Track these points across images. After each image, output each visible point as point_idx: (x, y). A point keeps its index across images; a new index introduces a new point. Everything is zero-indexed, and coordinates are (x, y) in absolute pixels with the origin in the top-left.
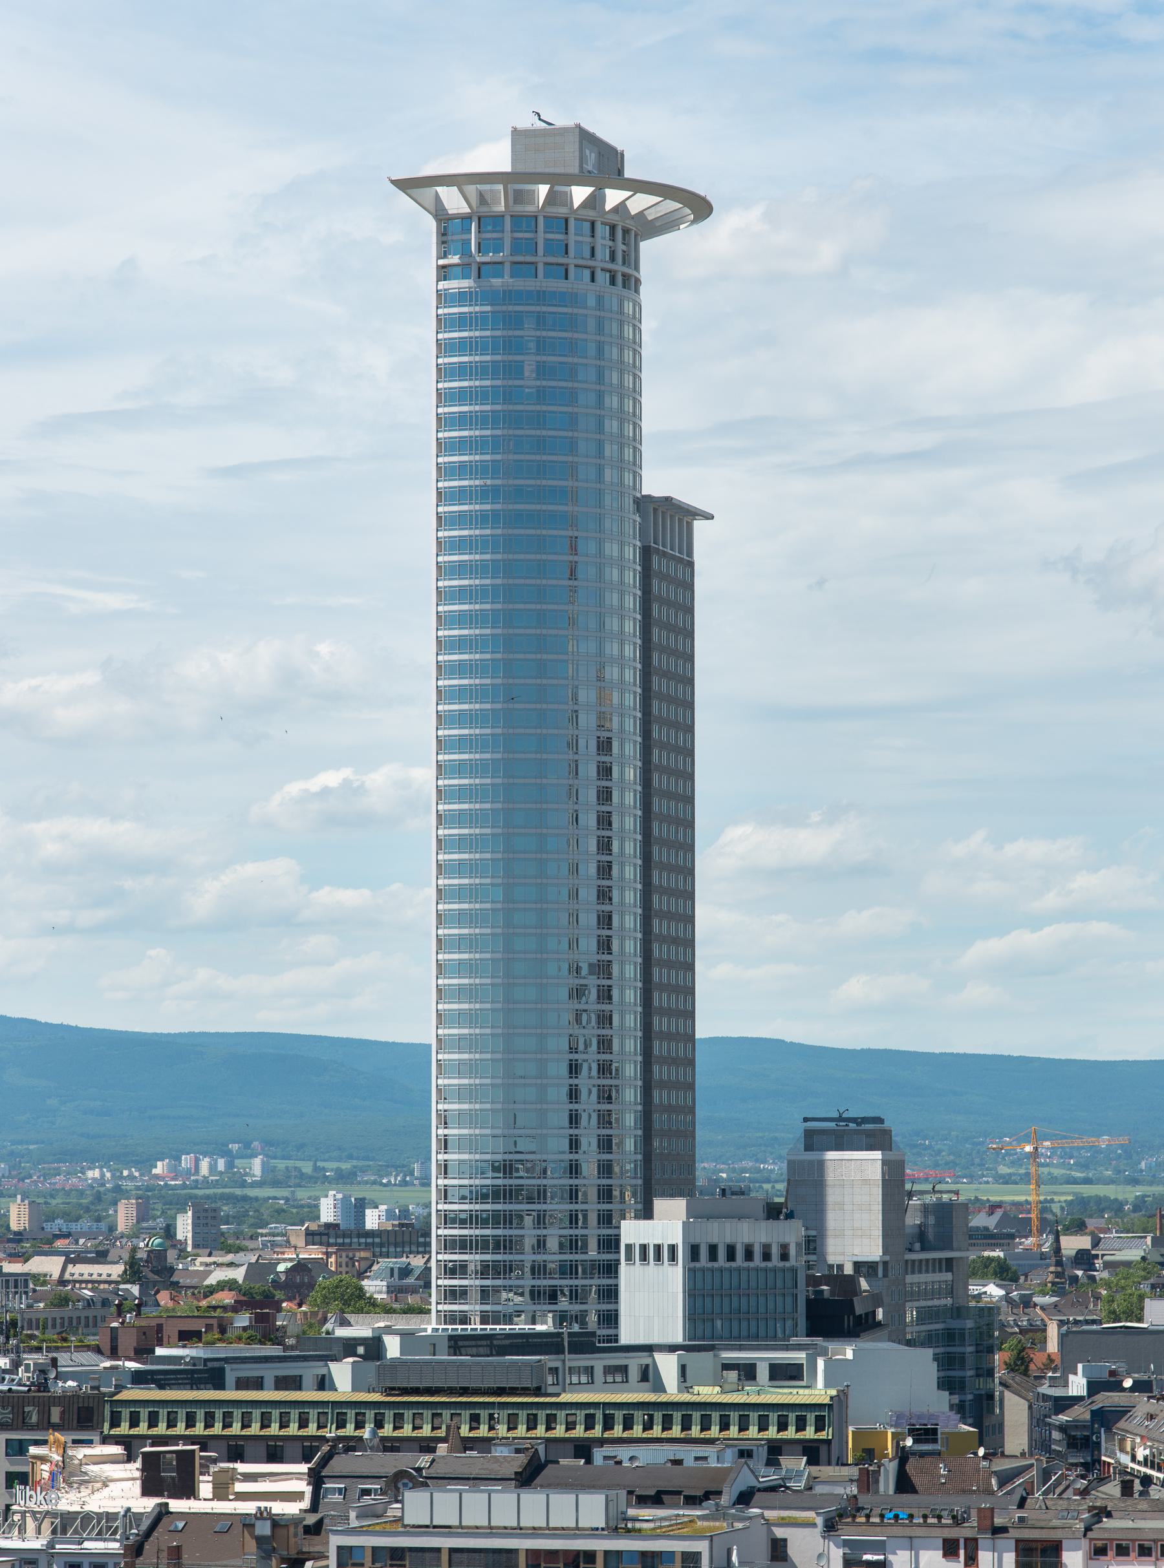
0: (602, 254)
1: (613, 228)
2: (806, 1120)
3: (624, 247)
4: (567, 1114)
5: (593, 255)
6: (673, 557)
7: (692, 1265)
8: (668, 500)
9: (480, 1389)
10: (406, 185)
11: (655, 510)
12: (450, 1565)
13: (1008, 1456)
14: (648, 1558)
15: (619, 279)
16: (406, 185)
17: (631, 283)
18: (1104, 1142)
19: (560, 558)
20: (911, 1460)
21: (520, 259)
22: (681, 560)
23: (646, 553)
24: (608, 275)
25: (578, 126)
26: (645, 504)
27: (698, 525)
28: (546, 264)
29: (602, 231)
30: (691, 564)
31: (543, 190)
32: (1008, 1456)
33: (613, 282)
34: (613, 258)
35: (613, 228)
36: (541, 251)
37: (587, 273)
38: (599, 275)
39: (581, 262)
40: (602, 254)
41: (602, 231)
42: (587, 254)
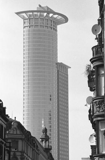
2: (82, 158)
5: (48, 24)
6: (64, 73)
8: (61, 63)
10: (18, 13)
11: (60, 65)
12: (58, 159)
14: (103, 114)
16: (18, 13)
17: (56, 30)
18: (43, 122)
21: (36, 25)
22: (66, 74)
23: (58, 71)
25: (47, 6)
26: (57, 64)
27: (69, 69)
28: (40, 26)
30: (68, 75)
34: (51, 25)
36: (39, 24)
37: (47, 27)
39: (46, 25)
42: (47, 24)
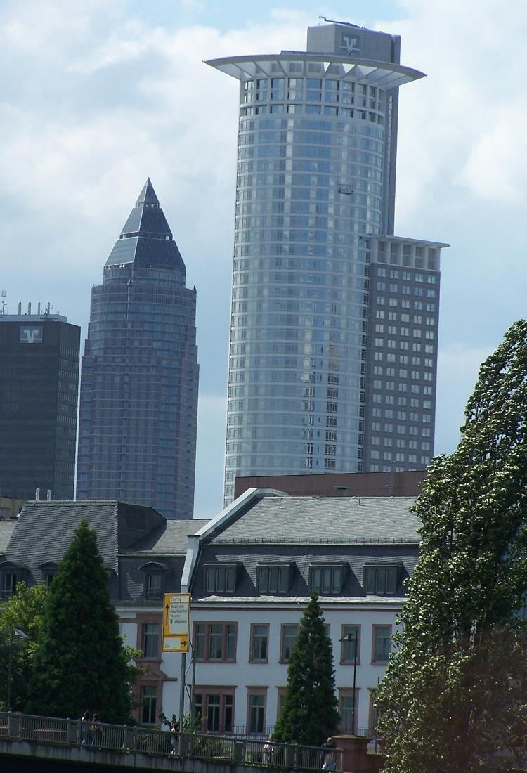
0: (358, 101)
1: (365, 87)
3: (372, 98)
4: (338, 425)
7: (262, 707)
9: (384, 175)
13: (194, 666)
15: (368, 116)
19: (260, 454)
20: (261, 81)
24: (362, 87)
29: (358, 88)
31: (326, 65)
32: (194, 666)
33: (364, 118)
34: (364, 104)
35: (365, 87)
36: (323, 98)
38: (356, 113)
40: (358, 101)
41: (358, 88)
